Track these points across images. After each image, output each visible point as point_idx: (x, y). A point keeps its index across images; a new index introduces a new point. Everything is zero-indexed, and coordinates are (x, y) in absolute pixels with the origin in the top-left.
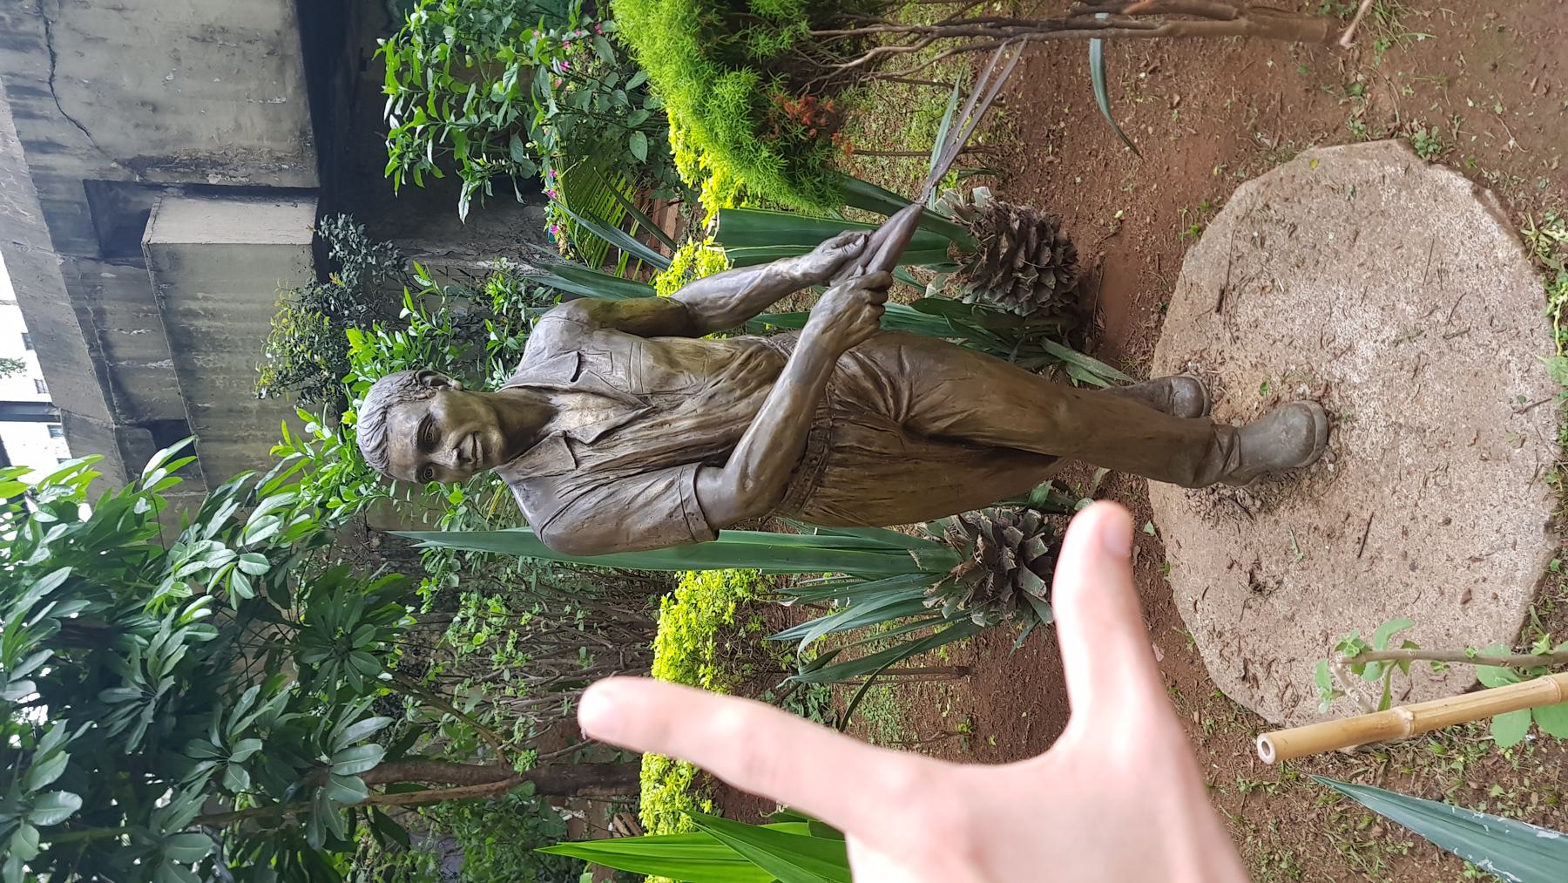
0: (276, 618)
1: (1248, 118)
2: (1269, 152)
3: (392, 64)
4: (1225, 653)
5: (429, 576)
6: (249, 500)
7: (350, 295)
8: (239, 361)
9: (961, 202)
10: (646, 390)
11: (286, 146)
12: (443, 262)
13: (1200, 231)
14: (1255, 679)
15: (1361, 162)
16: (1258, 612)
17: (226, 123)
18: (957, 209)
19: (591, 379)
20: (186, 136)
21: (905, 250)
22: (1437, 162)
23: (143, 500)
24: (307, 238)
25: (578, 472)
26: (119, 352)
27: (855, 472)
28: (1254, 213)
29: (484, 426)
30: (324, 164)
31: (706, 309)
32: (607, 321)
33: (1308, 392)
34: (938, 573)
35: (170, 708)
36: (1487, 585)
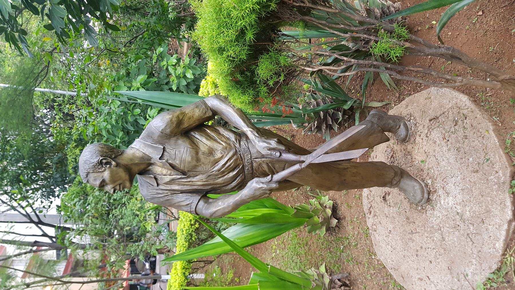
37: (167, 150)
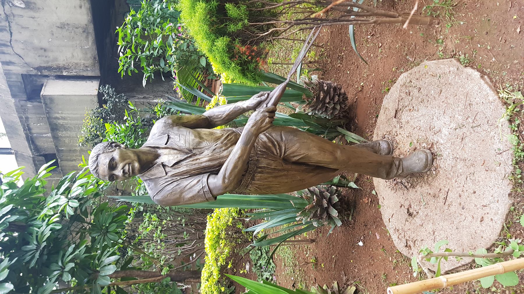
0: (83, 221)
1: (404, 51)
2: (411, 63)
3: (121, 35)
4: (400, 237)
5: (133, 207)
6: (73, 181)
7: (109, 111)
8: (73, 134)
9: (307, 80)
10: (191, 147)
11: (89, 62)
12: (142, 100)
13: (389, 90)
14: (410, 246)
15: (442, 66)
16: (410, 223)
17: (69, 55)
18: (306, 83)
19: (172, 144)
20: (56, 59)
21: (283, 97)
22: (468, 66)
23: (38, 182)
24: (96, 93)
25: (167, 177)
26: (33, 131)
27: (266, 175)
28: (406, 84)
29: (133, 161)
30: (101, 69)
31: (214, 118)
32: (179, 123)
33: (426, 146)
34: (301, 208)
35: (45, 252)
36: (489, 215)
37: (171, 136)
